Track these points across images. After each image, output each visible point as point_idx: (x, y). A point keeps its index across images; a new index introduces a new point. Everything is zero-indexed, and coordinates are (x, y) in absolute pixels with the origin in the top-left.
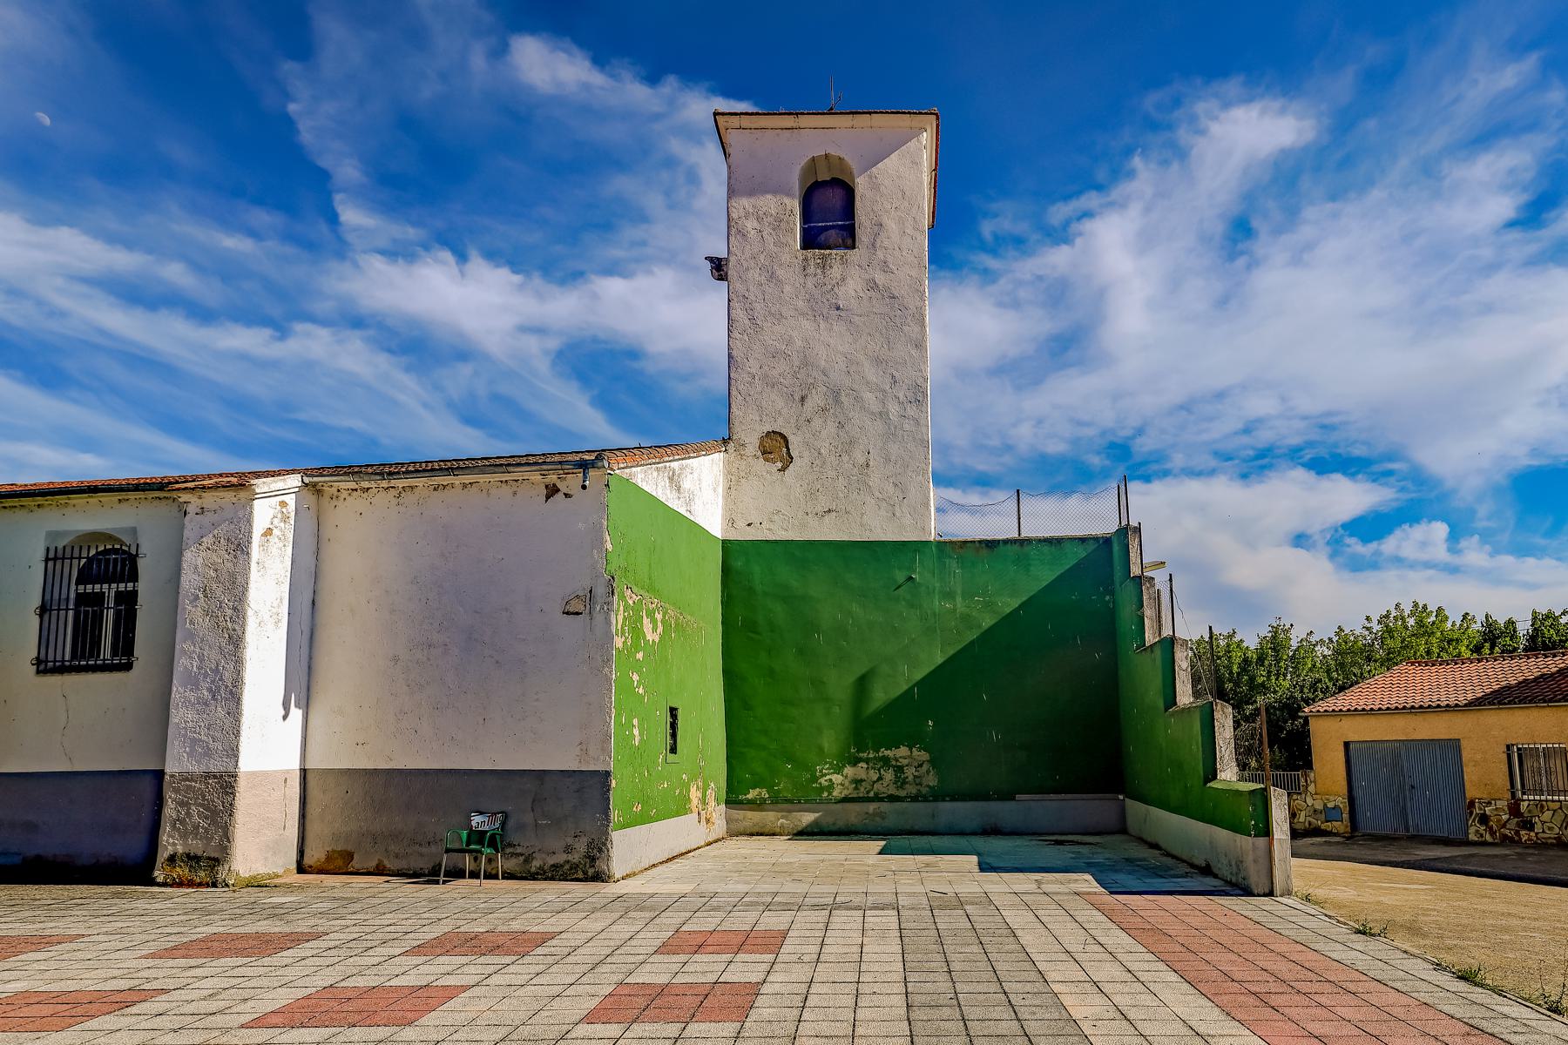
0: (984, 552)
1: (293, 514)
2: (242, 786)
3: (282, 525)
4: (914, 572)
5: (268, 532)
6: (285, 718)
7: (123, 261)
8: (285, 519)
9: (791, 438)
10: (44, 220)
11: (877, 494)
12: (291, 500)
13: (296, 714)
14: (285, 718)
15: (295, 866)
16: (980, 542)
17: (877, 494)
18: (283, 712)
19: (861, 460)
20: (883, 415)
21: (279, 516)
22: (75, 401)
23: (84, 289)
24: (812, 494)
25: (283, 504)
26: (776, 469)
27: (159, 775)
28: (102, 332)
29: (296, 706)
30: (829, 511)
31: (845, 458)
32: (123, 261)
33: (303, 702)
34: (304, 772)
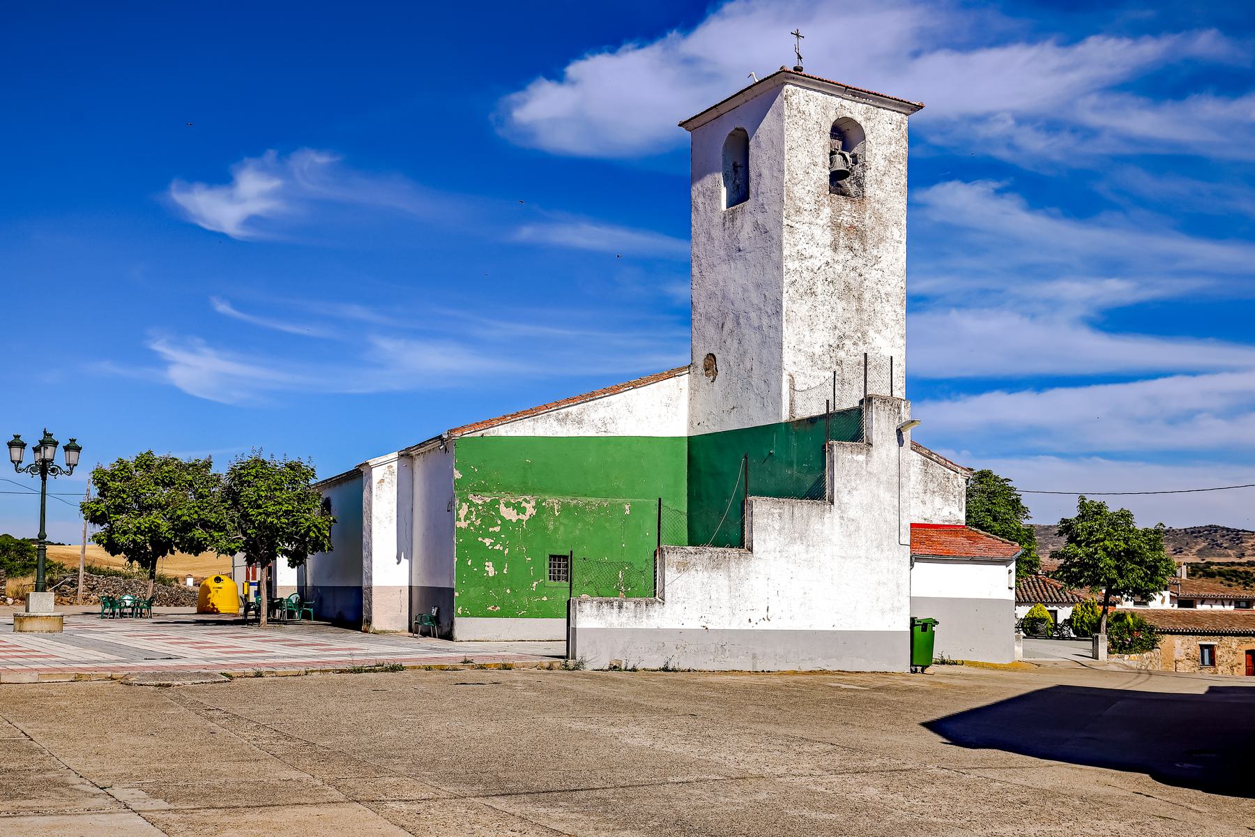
0: (809, 428)
1: (396, 471)
2: (373, 590)
3: (390, 476)
4: (772, 449)
5: (382, 481)
6: (398, 563)
7: (1149, 50)
8: (392, 473)
9: (717, 356)
10: (1072, 39)
11: (756, 390)
12: (395, 464)
13: (405, 562)
14: (398, 563)
15: (408, 629)
16: (807, 419)
17: (756, 390)
18: (397, 561)
19: (749, 367)
20: (760, 328)
21: (388, 473)
22: (1105, 226)
23: (1116, 99)
24: (725, 397)
25: (391, 467)
26: (710, 381)
27: (361, 588)
28: (1130, 140)
29: (405, 558)
30: (733, 408)
31: (741, 366)
32: (1149, 50)
33: (409, 556)
34: (410, 587)
